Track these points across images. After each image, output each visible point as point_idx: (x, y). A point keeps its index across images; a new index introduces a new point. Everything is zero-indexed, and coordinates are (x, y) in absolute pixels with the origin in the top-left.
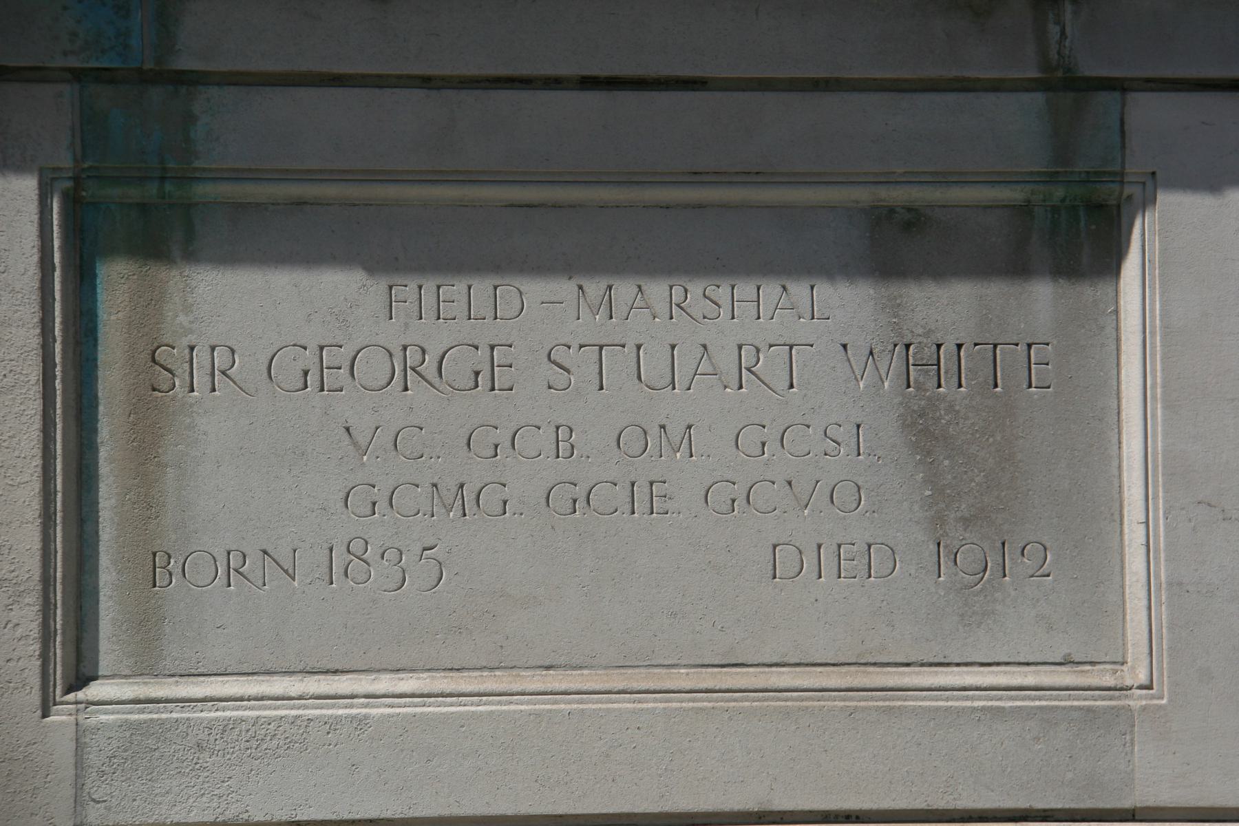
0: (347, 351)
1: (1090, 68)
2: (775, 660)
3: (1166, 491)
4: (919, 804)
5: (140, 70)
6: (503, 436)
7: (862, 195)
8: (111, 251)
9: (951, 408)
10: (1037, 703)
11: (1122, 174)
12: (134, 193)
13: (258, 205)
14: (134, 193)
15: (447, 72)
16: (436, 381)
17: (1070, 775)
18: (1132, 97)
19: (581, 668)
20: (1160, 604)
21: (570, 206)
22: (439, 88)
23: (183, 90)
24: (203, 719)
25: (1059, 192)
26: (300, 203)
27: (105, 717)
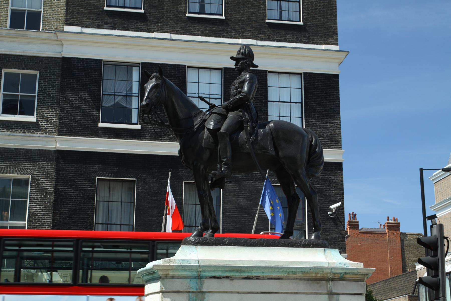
1: (334, 291)
15: (241, 291)
18: (340, 296)
23: (204, 294)
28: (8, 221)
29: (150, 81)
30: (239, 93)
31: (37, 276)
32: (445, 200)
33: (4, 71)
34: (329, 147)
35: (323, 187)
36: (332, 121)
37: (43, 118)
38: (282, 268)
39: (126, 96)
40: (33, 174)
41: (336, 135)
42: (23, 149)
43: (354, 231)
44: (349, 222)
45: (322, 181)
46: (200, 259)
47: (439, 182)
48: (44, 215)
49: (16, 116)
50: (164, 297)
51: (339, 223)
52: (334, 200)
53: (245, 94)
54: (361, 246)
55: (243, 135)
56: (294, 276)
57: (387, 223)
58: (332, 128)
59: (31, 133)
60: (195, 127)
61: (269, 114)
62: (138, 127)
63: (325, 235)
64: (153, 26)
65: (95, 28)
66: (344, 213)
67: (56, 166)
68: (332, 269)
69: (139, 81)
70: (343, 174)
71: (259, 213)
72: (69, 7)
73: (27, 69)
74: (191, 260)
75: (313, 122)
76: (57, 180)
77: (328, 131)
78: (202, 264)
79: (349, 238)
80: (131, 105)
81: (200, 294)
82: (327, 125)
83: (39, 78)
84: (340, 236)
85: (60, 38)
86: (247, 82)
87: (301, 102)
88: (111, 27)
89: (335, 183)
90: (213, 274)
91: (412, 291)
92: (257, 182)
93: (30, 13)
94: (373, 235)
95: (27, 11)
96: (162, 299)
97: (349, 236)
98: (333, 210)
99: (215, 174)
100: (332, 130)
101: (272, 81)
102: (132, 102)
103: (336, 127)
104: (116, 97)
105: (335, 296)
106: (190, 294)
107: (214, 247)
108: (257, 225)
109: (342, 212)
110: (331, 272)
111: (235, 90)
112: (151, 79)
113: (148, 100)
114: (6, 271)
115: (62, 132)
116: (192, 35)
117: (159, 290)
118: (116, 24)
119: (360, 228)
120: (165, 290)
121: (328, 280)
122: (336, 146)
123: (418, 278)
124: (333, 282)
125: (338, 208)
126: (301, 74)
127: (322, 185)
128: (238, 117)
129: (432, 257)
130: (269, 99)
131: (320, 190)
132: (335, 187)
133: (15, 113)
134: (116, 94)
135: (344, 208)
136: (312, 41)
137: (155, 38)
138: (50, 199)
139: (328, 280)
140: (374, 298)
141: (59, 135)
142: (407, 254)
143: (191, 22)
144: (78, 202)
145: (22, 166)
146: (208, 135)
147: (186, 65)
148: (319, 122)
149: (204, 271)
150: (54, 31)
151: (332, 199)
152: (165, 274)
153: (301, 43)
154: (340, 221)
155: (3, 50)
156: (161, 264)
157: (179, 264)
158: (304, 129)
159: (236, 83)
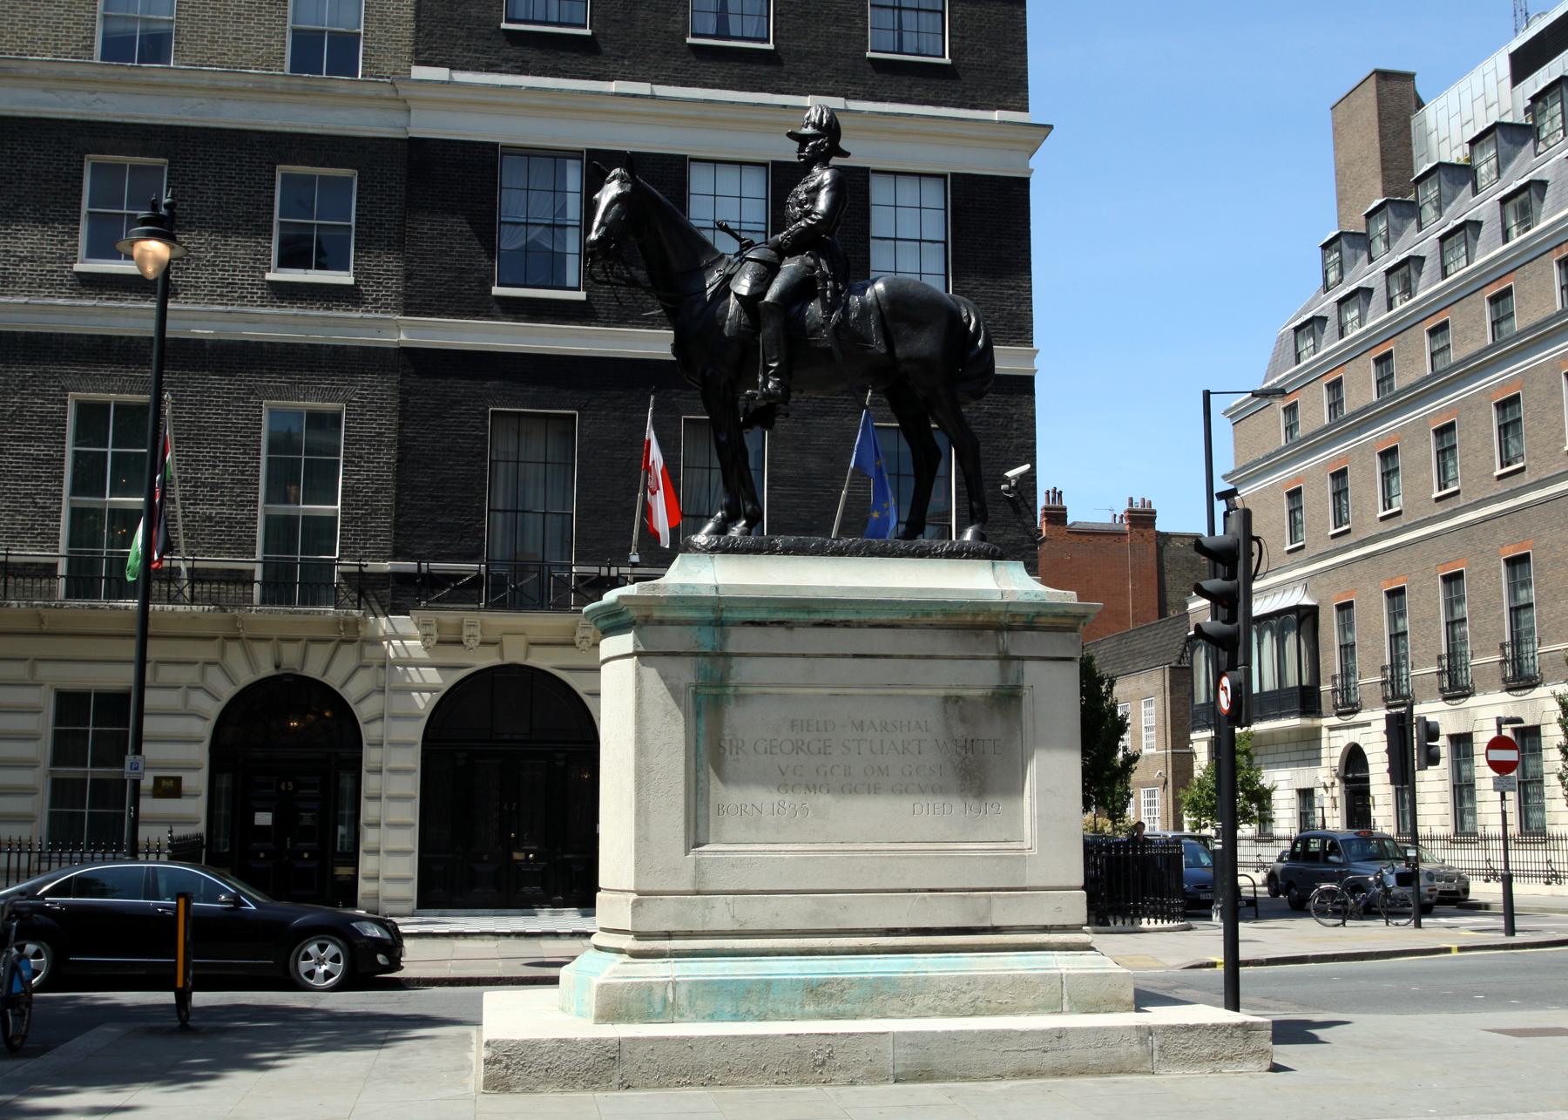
1: (1013, 653)
28: (299, 504)
29: (607, 186)
30: (808, 214)
31: (366, 622)
32: (1255, 461)
33: (281, 170)
34: (1006, 343)
37: (369, 276)
38: (899, 603)
39: (553, 226)
40: (350, 401)
42: (328, 346)
43: (1056, 527)
44: (1046, 508)
46: (720, 582)
48: (377, 491)
49: (309, 271)
50: (643, 665)
51: (1024, 509)
53: (820, 217)
54: (1070, 561)
55: (815, 308)
56: (926, 620)
57: (1129, 511)
59: (344, 310)
60: (709, 291)
61: (872, 267)
62: (581, 295)
64: (612, 67)
65: (481, 71)
67: (401, 382)
68: (1008, 604)
69: (581, 193)
71: (848, 488)
72: (422, 24)
73: (332, 166)
74: (700, 585)
76: (403, 415)
78: (724, 594)
79: (1046, 545)
80: (565, 246)
81: (721, 660)
83: (358, 186)
85: (402, 94)
86: (826, 189)
87: (943, 239)
88: (518, 67)
89: (1017, 421)
90: (749, 616)
91: (1177, 658)
92: (846, 419)
93: (334, 36)
94: (1098, 537)
95: (330, 32)
96: (637, 669)
97: (1045, 539)
99: (753, 397)
101: (880, 191)
102: (565, 239)
104: (531, 228)
105: (1015, 663)
106: (700, 659)
107: (751, 556)
108: (844, 514)
110: (1006, 612)
111: (797, 209)
112: (610, 182)
113: (603, 229)
114: (300, 612)
115: (410, 308)
116: (700, 87)
117: (630, 650)
118: (529, 62)
119: (1069, 521)
121: (1000, 628)
123: (1192, 626)
124: (1011, 633)
125: (1022, 475)
126: (944, 176)
128: (804, 268)
129: (1224, 579)
130: (874, 232)
132: (1017, 429)
133: (307, 266)
134: (530, 221)
136: (970, 102)
137: (616, 94)
138: (388, 456)
139: (1000, 628)
140: (1097, 671)
141: (406, 314)
142: (1168, 578)
143: (697, 57)
144: (451, 463)
145: (325, 384)
146: (736, 310)
147: (685, 156)
149: (730, 609)
150: (388, 78)
153: (946, 106)
154: (1027, 505)
155: (276, 122)
156: (635, 593)
157: (675, 594)
158: (950, 297)
159: (801, 191)
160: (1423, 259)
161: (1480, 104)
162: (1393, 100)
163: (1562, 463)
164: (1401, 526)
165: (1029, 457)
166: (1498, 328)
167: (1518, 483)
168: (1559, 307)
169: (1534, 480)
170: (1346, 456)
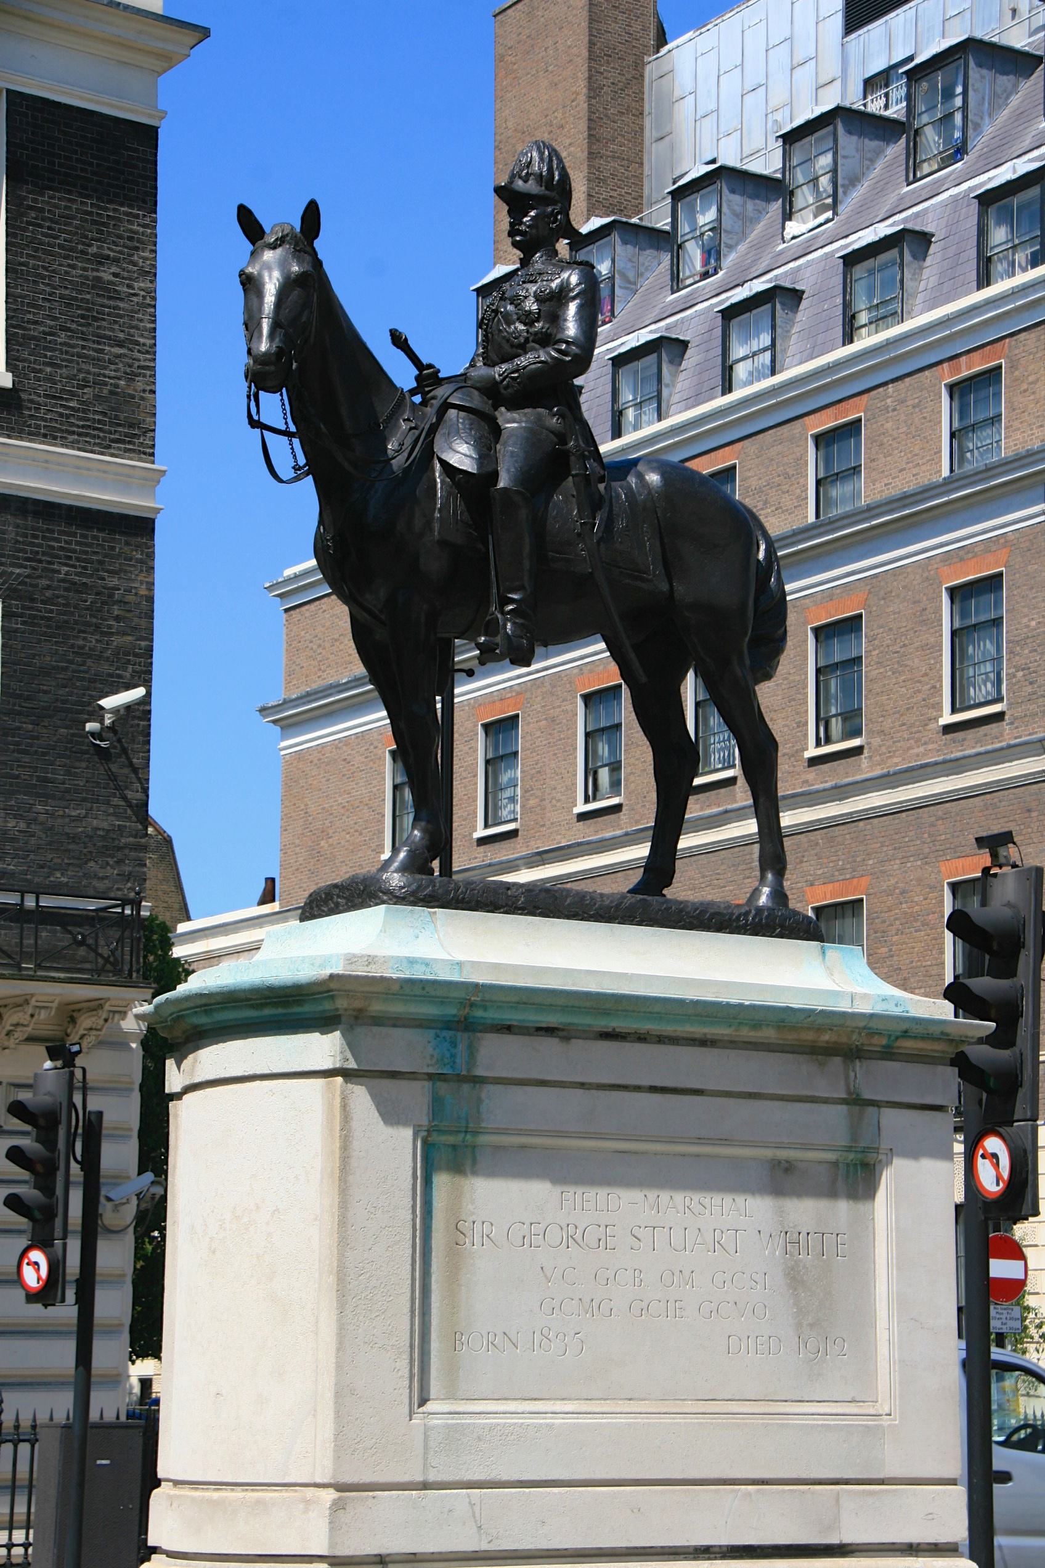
0: (542, 1226)
1: (867, 1095)
2: (729, 1397)
3: (898, 1313)
4: (794, 1476)
5: (458, 1075)
6: (610, 1274)
7: (769, 1153)
8: (440, 1169)
9: (804, 1267)
10: (844, 1423)
11: (878, 1149)
12: (451, 1139)
13: (505, 1147)
14: (451, 1139)
16: (581, 1243)
17: (858, 1461)
18: (883, 1109)
19: (645, 1400)
20: (895, 1371)
21: (642, 1153)
22: (589, 1089)
23: (478, 1086)
24: (481, 1424)
25: (851, 1156)
26: (523, 1147)
27: (436, 1422)
32: (331, 687)
35: (72, 614)
36: (121, 335)
41: (133, 397)
45: (66, 590)
47: (307, 607)
52: (111, 676)
58: (121, 365)
63: (67, 820)
66: (149, 735)
70: (153, 568)
75: (42, 329)
77: (105, 376)
81: (466, 1088)
82: (101, 351)
84: (125, 826)
98: (107, 716)
100: (118, 374)
103: (137, 364)
105: (871, 1110)
109: (141, 728)
110: (864, 1028)
120: (356, 1067)
121: (852, 1054)
122: (134, 444)
125: (128, 707)
127: (67, 605)
131: (58, 628)
135: (149, 712)
139: (852, 1054)
148: (69, 329)
151: (105, 668)
152: (354, 1010)
160: (684, 345)
161: (780, 56)
162: (615, 20)
163: (930, 747)
164: (618, 832)
165: (140, 673)
166: (825, 494)
167: (847, 775)
168: (945, 472)
169: (877, 772)
170: (519, 693)
